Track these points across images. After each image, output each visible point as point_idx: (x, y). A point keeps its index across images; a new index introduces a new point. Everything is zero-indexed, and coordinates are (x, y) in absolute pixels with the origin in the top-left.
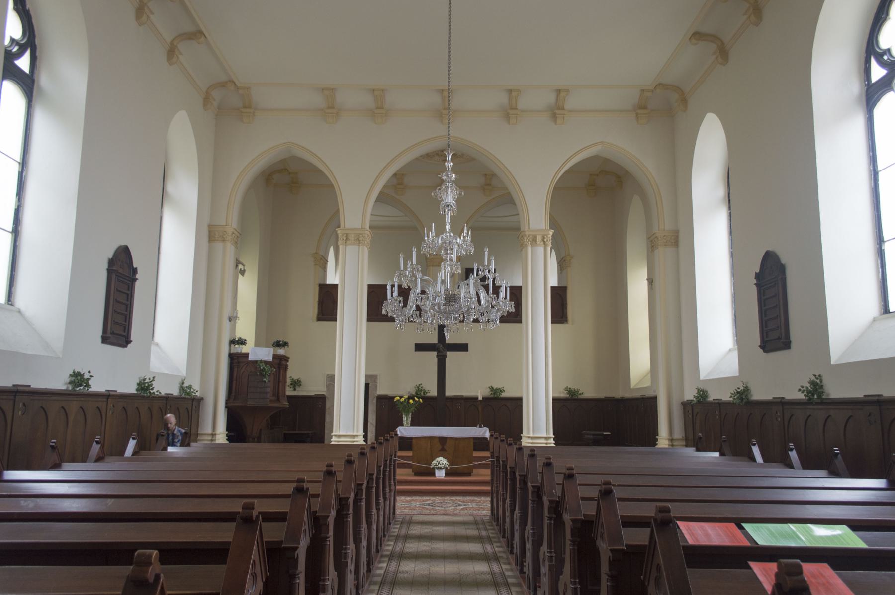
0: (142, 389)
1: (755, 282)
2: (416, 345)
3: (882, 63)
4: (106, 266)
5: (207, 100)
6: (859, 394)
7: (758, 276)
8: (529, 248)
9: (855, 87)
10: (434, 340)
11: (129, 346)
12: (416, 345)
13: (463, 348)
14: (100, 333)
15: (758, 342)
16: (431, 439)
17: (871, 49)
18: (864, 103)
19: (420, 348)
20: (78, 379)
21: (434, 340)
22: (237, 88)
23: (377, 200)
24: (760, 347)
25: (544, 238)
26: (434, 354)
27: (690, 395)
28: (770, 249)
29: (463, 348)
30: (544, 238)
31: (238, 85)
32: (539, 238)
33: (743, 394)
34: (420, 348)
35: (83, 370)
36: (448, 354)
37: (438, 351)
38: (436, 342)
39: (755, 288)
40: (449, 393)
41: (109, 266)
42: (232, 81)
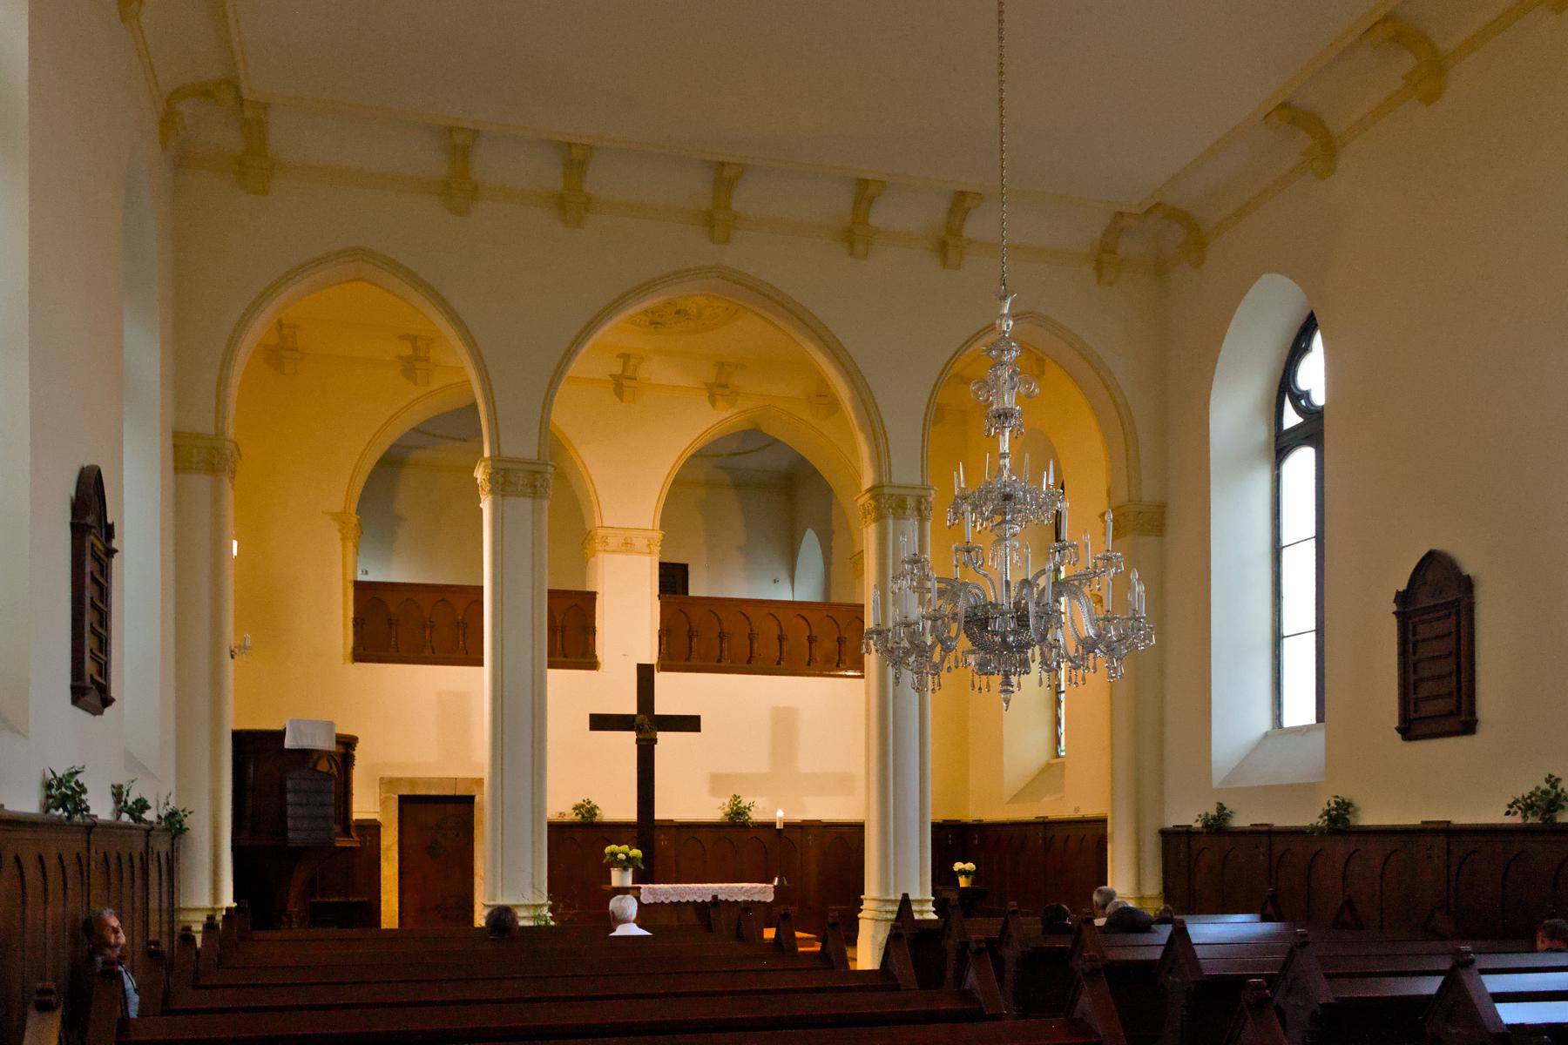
0: (62, 802)
1: (1395, 608)
2: (592, 717)
3: (1299, 410)
4: (67, 517)
5: (168, 122)
6: (1413, 819)
7: (1402, 599)
8: (891, 522)
9: (1262, 433)
10: (630, 707)
11: (107, 710)
12: (592, 717)
13: (690, 724)
14: (68, 681)
15: (1394, 721)
16: (677, 906)
17: (1286, 386)
18: (1273, 454)
19: (600, 722)
20: (1339, 818)
21: (630, 707)
22: (240, 100)
23: (474, 406)
24: (1399, 730)
25: (919, 502)
26: (631, 736)
27: (1188, 814)
28: (1438, 546)
29: (690, 724)
30: (919, 502)
31: (246, 95)
32: (911, 503)
33: (1339, 818)
34: (600, 722)
35: (1346, 795)
36: (660, 735)
37: (639, 730)
38: (632, 709)
39: (1394, 621)
40: (659, 815)
41: (74, 515)
42: (233, 84)
